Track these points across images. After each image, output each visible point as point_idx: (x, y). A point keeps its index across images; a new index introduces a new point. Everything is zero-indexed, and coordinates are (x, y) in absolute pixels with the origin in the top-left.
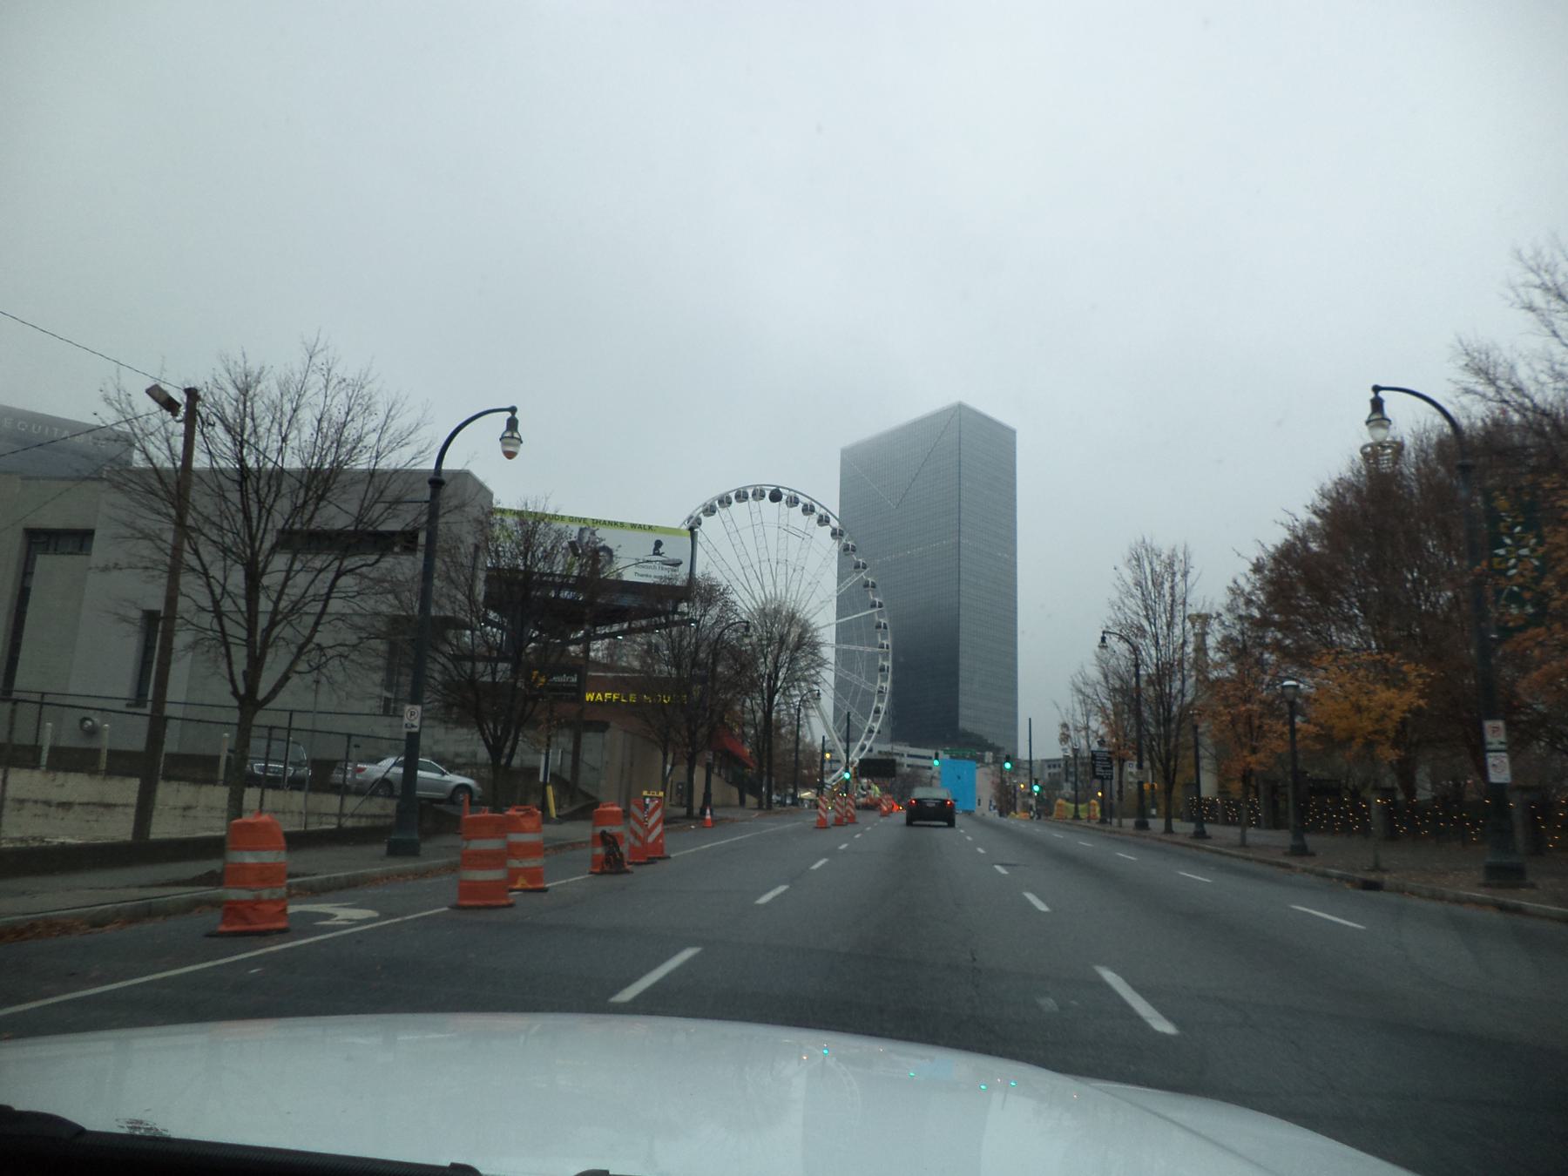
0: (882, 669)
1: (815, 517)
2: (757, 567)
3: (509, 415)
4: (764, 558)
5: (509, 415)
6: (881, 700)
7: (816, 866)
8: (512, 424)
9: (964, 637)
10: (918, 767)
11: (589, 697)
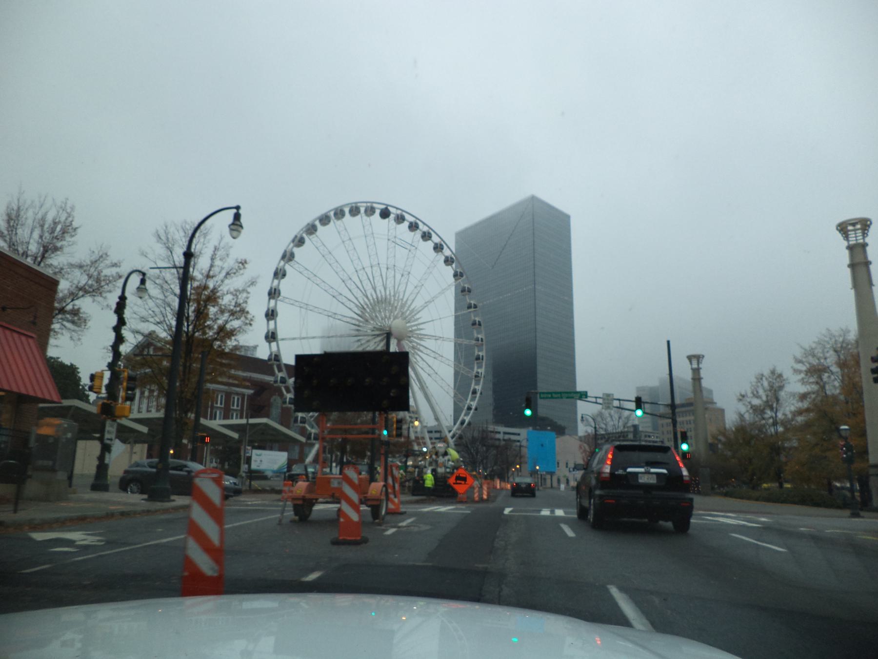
0: (478, 358)
1: (406, 224)
2: (369, 270)
3: (235, 211)
4: (375, 263)
5: (235, 211)
6: (477, 383)
7: (846, 427)
8: (237, 217)
9: (540, 361)
10: (509, 440)
11: (221, 448)
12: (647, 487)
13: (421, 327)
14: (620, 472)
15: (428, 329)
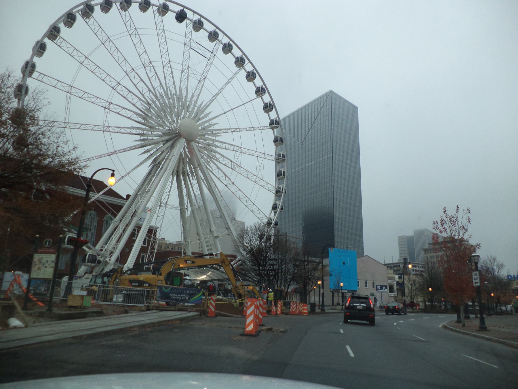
12: (360, 310)
13: (213, 122)
14: (352, 305)
15: (221, 123)
